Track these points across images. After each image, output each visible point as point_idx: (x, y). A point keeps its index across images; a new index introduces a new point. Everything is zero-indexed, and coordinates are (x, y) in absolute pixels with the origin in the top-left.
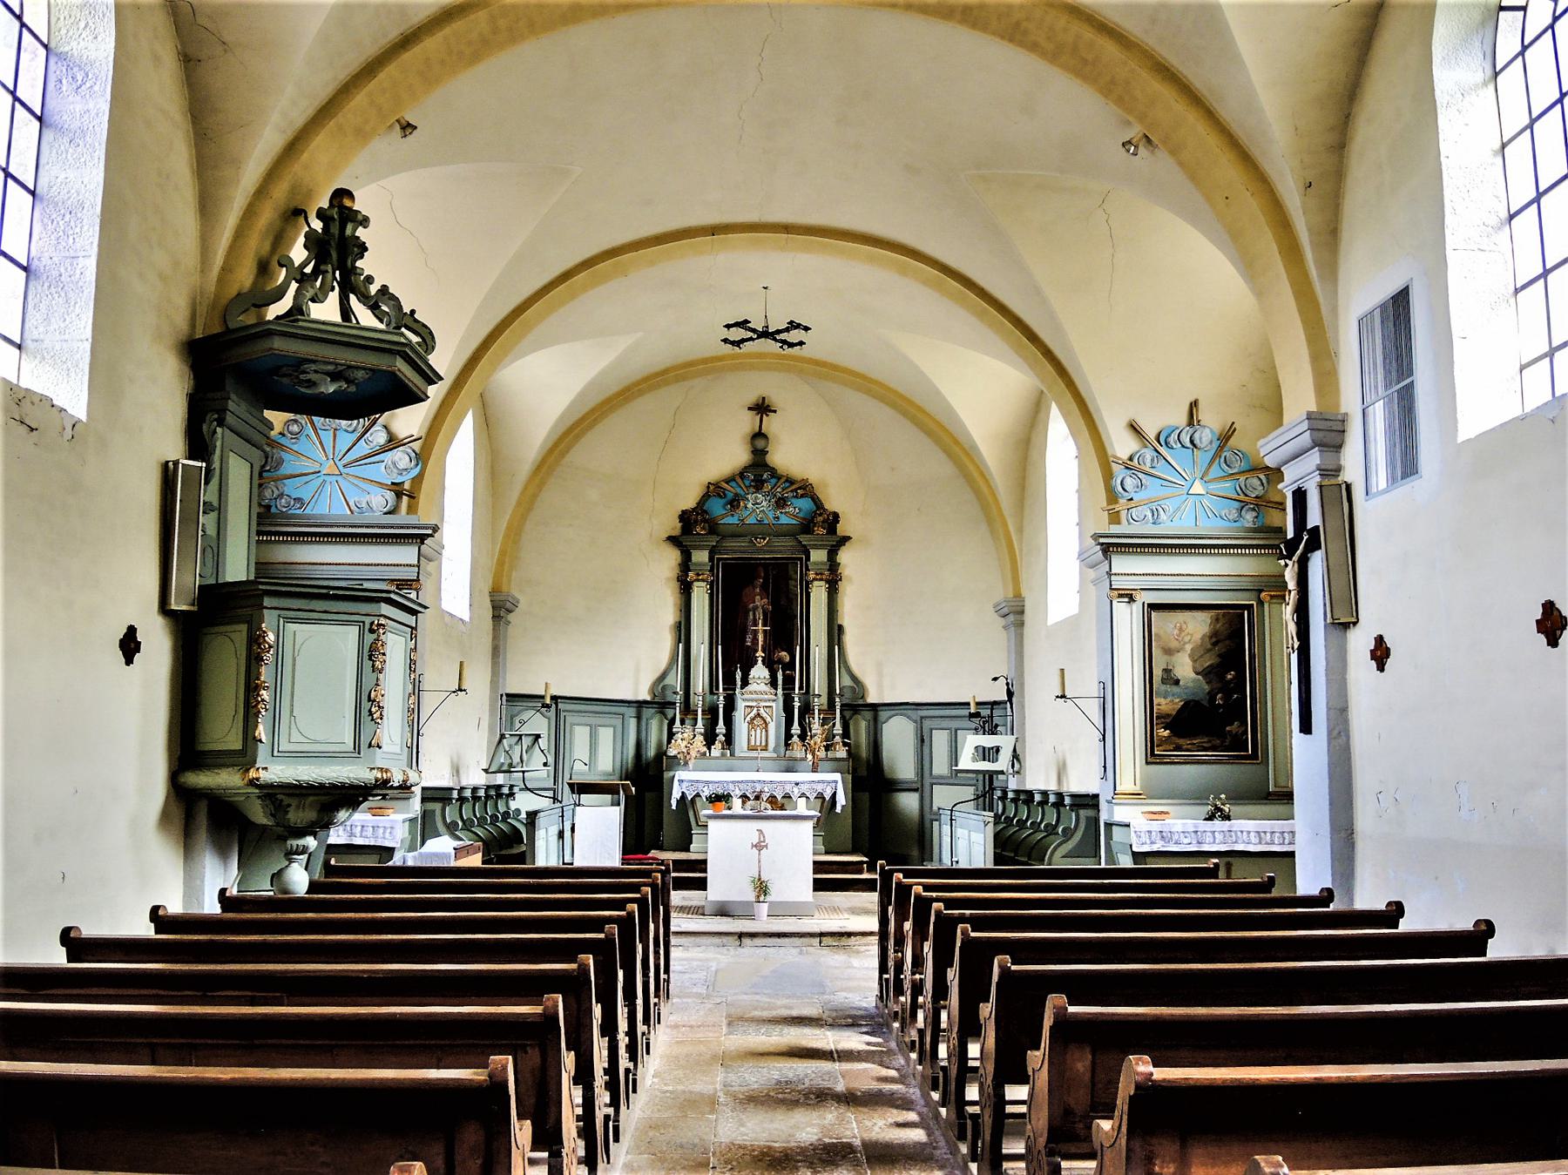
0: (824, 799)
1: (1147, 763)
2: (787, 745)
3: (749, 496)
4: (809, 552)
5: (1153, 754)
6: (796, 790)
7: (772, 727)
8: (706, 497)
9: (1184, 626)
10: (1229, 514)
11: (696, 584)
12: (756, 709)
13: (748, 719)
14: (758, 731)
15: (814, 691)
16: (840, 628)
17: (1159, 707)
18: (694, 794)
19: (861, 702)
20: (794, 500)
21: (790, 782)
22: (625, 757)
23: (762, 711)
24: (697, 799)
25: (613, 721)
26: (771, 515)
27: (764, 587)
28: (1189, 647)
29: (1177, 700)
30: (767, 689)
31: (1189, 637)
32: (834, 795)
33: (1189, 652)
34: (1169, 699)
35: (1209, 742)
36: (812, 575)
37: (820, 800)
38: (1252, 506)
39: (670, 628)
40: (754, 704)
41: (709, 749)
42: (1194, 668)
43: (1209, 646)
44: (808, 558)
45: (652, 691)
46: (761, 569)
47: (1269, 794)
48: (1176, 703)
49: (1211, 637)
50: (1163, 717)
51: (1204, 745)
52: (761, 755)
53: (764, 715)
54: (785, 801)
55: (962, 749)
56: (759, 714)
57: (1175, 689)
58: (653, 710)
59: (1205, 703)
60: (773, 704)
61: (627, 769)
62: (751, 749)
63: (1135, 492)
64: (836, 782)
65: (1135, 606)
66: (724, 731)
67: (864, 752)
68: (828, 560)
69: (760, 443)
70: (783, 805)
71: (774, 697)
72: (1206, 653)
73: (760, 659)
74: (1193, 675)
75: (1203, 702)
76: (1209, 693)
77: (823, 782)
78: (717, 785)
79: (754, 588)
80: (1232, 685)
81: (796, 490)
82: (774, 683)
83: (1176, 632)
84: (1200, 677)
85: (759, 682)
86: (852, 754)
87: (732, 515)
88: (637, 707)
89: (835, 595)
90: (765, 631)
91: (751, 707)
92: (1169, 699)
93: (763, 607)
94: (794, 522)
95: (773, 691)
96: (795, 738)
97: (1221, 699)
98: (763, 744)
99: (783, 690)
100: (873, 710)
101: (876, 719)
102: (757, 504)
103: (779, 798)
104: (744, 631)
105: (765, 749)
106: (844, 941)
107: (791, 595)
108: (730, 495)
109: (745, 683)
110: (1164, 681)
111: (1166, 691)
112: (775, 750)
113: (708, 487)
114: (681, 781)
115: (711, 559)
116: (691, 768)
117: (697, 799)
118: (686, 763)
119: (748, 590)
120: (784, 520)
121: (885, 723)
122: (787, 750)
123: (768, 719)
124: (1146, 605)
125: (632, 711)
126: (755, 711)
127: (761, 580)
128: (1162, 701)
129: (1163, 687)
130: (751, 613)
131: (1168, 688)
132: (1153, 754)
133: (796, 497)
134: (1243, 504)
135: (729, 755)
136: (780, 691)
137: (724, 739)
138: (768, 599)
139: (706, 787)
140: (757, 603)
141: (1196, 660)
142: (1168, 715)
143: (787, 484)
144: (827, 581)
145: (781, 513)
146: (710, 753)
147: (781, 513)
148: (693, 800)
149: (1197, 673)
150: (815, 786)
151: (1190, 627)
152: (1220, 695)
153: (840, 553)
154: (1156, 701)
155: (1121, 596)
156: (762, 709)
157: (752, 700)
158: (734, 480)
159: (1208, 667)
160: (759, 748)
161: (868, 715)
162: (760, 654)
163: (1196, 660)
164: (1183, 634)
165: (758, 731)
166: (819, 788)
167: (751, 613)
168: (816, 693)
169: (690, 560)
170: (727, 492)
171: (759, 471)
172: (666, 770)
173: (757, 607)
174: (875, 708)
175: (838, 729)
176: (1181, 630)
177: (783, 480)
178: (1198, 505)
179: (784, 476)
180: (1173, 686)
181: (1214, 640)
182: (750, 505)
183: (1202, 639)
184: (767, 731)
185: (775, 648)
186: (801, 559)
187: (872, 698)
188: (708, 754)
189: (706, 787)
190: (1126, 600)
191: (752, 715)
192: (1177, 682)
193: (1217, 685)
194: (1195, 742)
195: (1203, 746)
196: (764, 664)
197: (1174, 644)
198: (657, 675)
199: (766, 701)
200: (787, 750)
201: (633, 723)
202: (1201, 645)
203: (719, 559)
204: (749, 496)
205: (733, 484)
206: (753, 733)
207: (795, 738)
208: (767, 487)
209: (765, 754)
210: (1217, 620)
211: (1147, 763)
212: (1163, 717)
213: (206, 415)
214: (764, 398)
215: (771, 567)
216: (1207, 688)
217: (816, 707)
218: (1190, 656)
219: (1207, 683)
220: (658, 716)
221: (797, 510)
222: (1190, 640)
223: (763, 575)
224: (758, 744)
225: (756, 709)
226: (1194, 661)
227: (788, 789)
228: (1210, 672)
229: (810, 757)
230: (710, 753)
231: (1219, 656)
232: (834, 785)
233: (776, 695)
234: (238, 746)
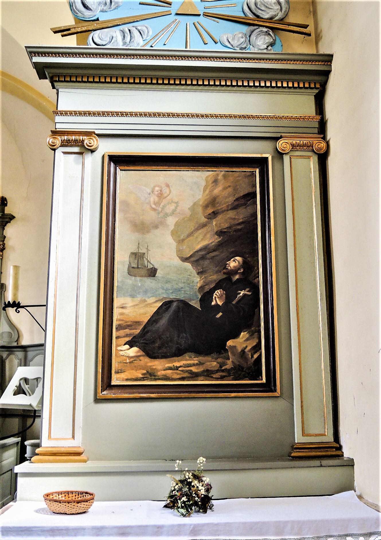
1: (97, 400)
5: (107, 385)
9: (166, 191)
10: (233, 39)
17: (121, 311)
28: (171, 221)
29: (152, 300)
31: (172, 207)
33: (172, 227)
34: (139, 298)
35: (200, 364)
38: (265, 30)
42: (179, 252)
43: (204, 220)
47: (294, 447)
48: (150, 305)
49: (206, 206)
50: (128, 326)
51: (194, 369)
55: (39, 383)
57: (149, 282)
59: (196, 304)
63: (102, 11)
65: (89, 158)
72: (197, 229)
74: (177, 261)
75: (192, 303)
76: (201, 288)
80: (237, 277)
83: (153, 198)
84: (188, 265)
92: (139, 298)
97: (220, 297)
100: (24, 351)
106: (60, 531)
110: (132, 271)
111: (134, 286)
124: (106, 159)
128: (129, 301)
129: (131, 281)
131: (138, 281)
132: (107, 385)
134: (252, 28)
141: (183, 240)
142: (138, 323)
149: (185, 260)
151: (174, 192)
154: (117, 302)
155: (65, 144)
159: (201, 250)
163: (183, 240)
164: (164, 202)
174: (24, 348)
176: (161, 195)
178: (191, 29)
180: (145, 279)
181: (210, 210)
183: (193, 208)
187: (25, 342)
190: (76, 149)
192: (152, 273)
193: (215, 277)
194: (177, 364)
195: (191, 372)
197: (150, 216)
202: (190, 219)
210: (216, 181)
211: (97, 400)
212: (128, 326)
213: (219, 317)
216: (198, 281)
218: (173, 233)
219: (198, 273)
222: (174, 211)
226: (181, 242)
228: (203, 258)
231: (220, 233)
234: (113, 383)
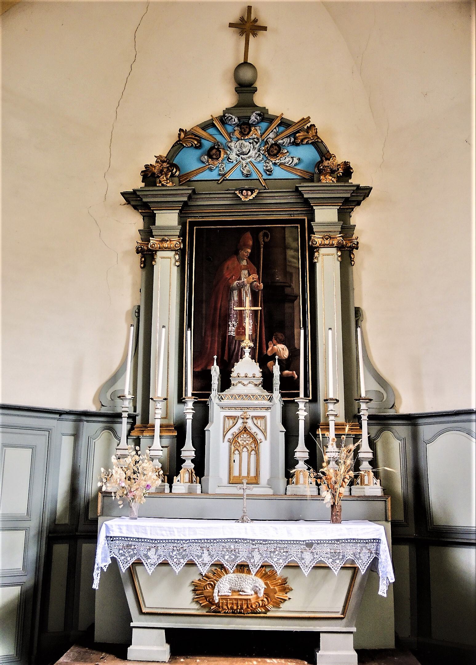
0: (355, 570)
2: (288, 476)
3: (232, 144)
4: (313, 211)
6: (308, 556)
7: (265, 448)
8: (178, 146)
11: (160, 254)
12: (240, 421)
13: (229, 436)
14: (245, 455)
15: (327, 393)
16: (358, 311)
18: (134, 560)
19: (391, 412)
20: (292, 149)
21: (297, 542)
22: (49, 499)
23: (250, 424)
24: (139, 569)
25: (29, 438)
26: (261, 167)
27: (253, 258)
30: (260, 391)
32: (375, 562)
36: (317, 239)
37: (349, 573)
39: (213, 422)
40: (238, 413)
41: (171, 482)
44: (312, 218)
45: (98, 398)
46: (249, 235)
52: (248, 492)
53: (254, 430)
54: (289, 573)
56: (245, 429)
58: (101, 425)
60: (267, 414)
61: (54, 512)
62: (233, 481)
64: (378, 541)
66: (193, 454)
67: (399, 487)
68: (339, 219)
69: (246, 75)
70: (285, 581)
71: (266, 403)
73: (247, 351)
77: (356, 541)
78: (171, 546)
79: (240, 260)
81: (294, 134)
82: (267, 384)
85: (245, 383)
86: (387, 491)
87: (211, 170)
88: (75, 421)
89: (350, 269)
90: (255, 312)
91: (234, 418)
93: (251, 284)
94: (295, 177)
95: (266, 393)
96: (301, 466)
98: (253, 474)
99: (283, 395)
101: (415, 437)
102: (243, 153)
103: (279, 571)
104: (226, 318)
105: (255, 481)
107: (289, 269)
108: (207, 145)
109: (225, 384)
112: (270, 484)
113: (179, 135)
114: (110, 539)
115: (182, 223)
116: (136, 514)
117: (139, 569)
118: (127, 505)
119: (231, 263)
120: (279, 173)
121: (430, 442)
122: (288, 483)
123: (260, 436)
125: (67, 425)
126: (239, 424)
127: (249, 251)
130: (235, 293)
133: (295, 144)
135: (199, 491)
136: (277, 394)
137: (193, 466)
138: (258, 274)
139: (153, 550)
140: (243, 279)
143: (282, 129)
144: (340, 247)
145: (275, 164)
146: (171, 487)
147: (275, 164)
148: (131, 572)
150: (339, 548)
152: (121, 507)
153: (353, 214)
156: (249, 421)
157: (235, 408)
158: (214, 126)
160: (245, 481)
161: (403, 430)
162: (247, 343)
165: (245, 455)
166: (349, 552)
167: (235, 293)
168: (331, 396)
169: (154, 224)
170: (203, 141)
171: (244, 112)
172: (102, 514)
173: (243, 285)
175: (366, 452)
177: (277, 122)
179: (278, 117)
182: (233, 156)
184: (257, 454)
185: (269, 339)
186: (302, 222)
187: (404, 409)
188: (167, 490)
189: (153, 550)
191: (235, 430)
196: (253, 357)
198: (106, 377)
199: (255, 408)
200: (288, 483)
201: (67, 443)
203: (192, 224)
204: (232, 144)
205: (211, 131)
206: (236, 457)
207: (301, 466)
208: (255, 133)
209: (255, 490)
214: (250, 8)
215: (261, 234)
217: (331, 418)
220: (106, 433)
221: (296, 161)
223: (251, 243)
224: (244, 474)
225: (240, 421)
227: (294, 555)
229: (327, 496)
230: (171, 487)
232: (373, 547)
233: (270, 399)
